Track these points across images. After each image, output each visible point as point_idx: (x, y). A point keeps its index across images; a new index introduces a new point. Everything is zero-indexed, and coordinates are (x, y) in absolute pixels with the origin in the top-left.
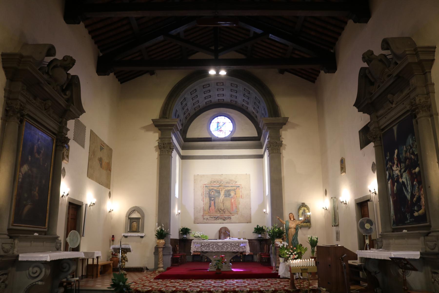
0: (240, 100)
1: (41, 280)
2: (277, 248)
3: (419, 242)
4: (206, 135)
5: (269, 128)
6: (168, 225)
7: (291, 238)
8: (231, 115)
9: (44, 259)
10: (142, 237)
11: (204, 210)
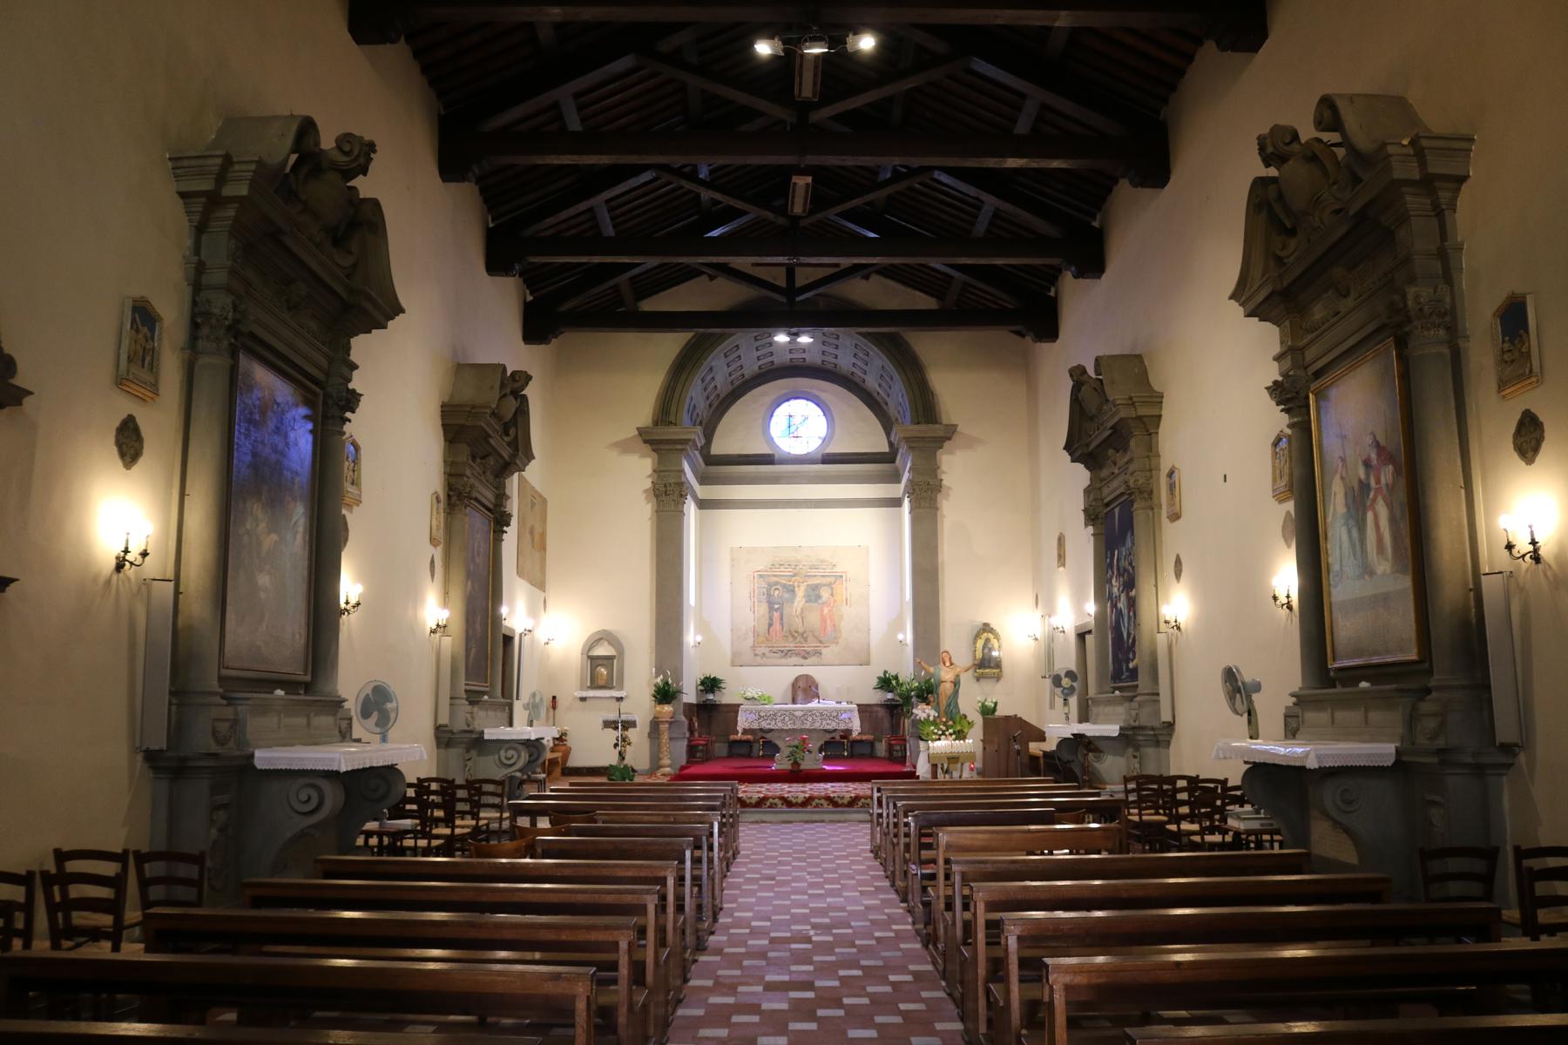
0: (845, 362)
1: (520, 770)
2: (917, 723)
3: (1120, 710)
4: (760, 448)
7: (944, 703)
8: (823, 395)
10: (620, 699)
11: (756, 634)
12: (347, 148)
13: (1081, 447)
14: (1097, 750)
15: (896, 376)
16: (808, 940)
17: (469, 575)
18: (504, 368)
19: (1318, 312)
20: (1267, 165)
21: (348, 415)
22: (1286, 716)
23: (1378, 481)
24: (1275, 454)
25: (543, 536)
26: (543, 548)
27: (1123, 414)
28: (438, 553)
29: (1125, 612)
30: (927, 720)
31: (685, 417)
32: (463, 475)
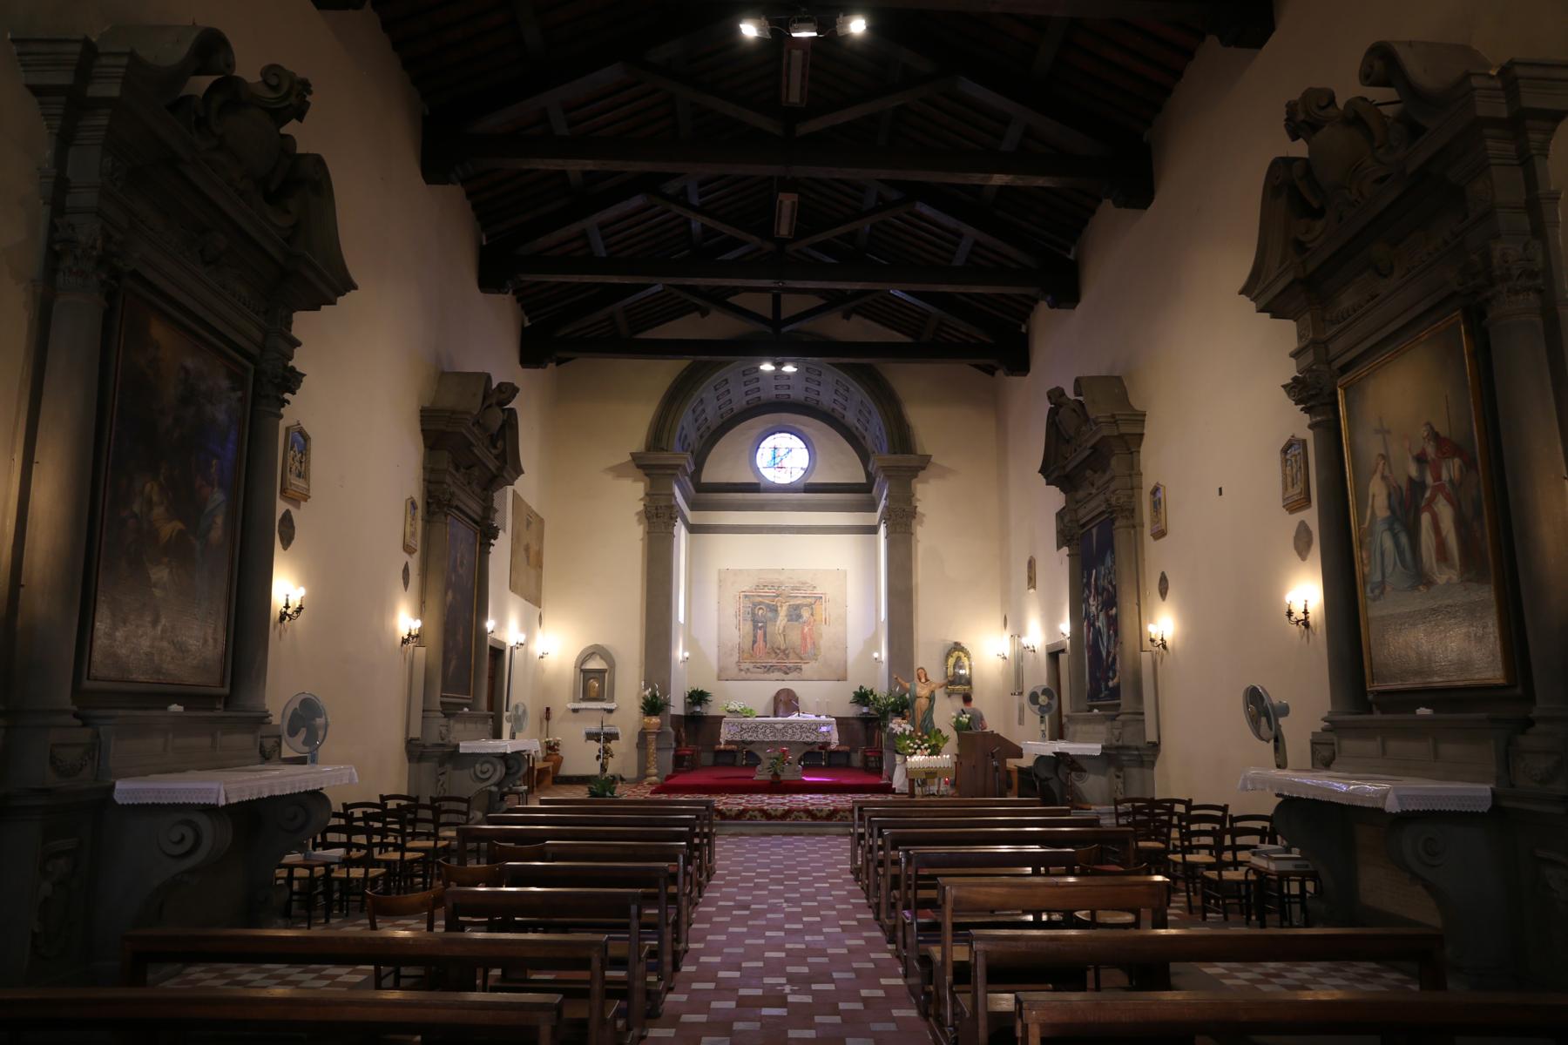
0: (827, 399)
2: (893, 736)
3: (1102, 729)
5: (888, 477)
6: (666, 689)
7: (919, 718)
8: (806, 430)
9: (501, 750)
10: (610, 711)
11: (741, 650)
12: (274, 81)
13: (1053, 471)
14: (1081, 770)
15: (874, 409)
16: (781, 1001)
17: (448, 586)
18: (488, 378)
19: (1347, 300)
20: (1294, 136)
21: (287, 396)
22: (1313, 743)
23: (1438, 478)
24: (1285, 462)
25: (539, 554)
26: (539, 565)
27: (1106, 432)
28: (414, 562)
29: (1104, 630)
30: (903, 734)
31: (676, 444)
32: (443, 482)
